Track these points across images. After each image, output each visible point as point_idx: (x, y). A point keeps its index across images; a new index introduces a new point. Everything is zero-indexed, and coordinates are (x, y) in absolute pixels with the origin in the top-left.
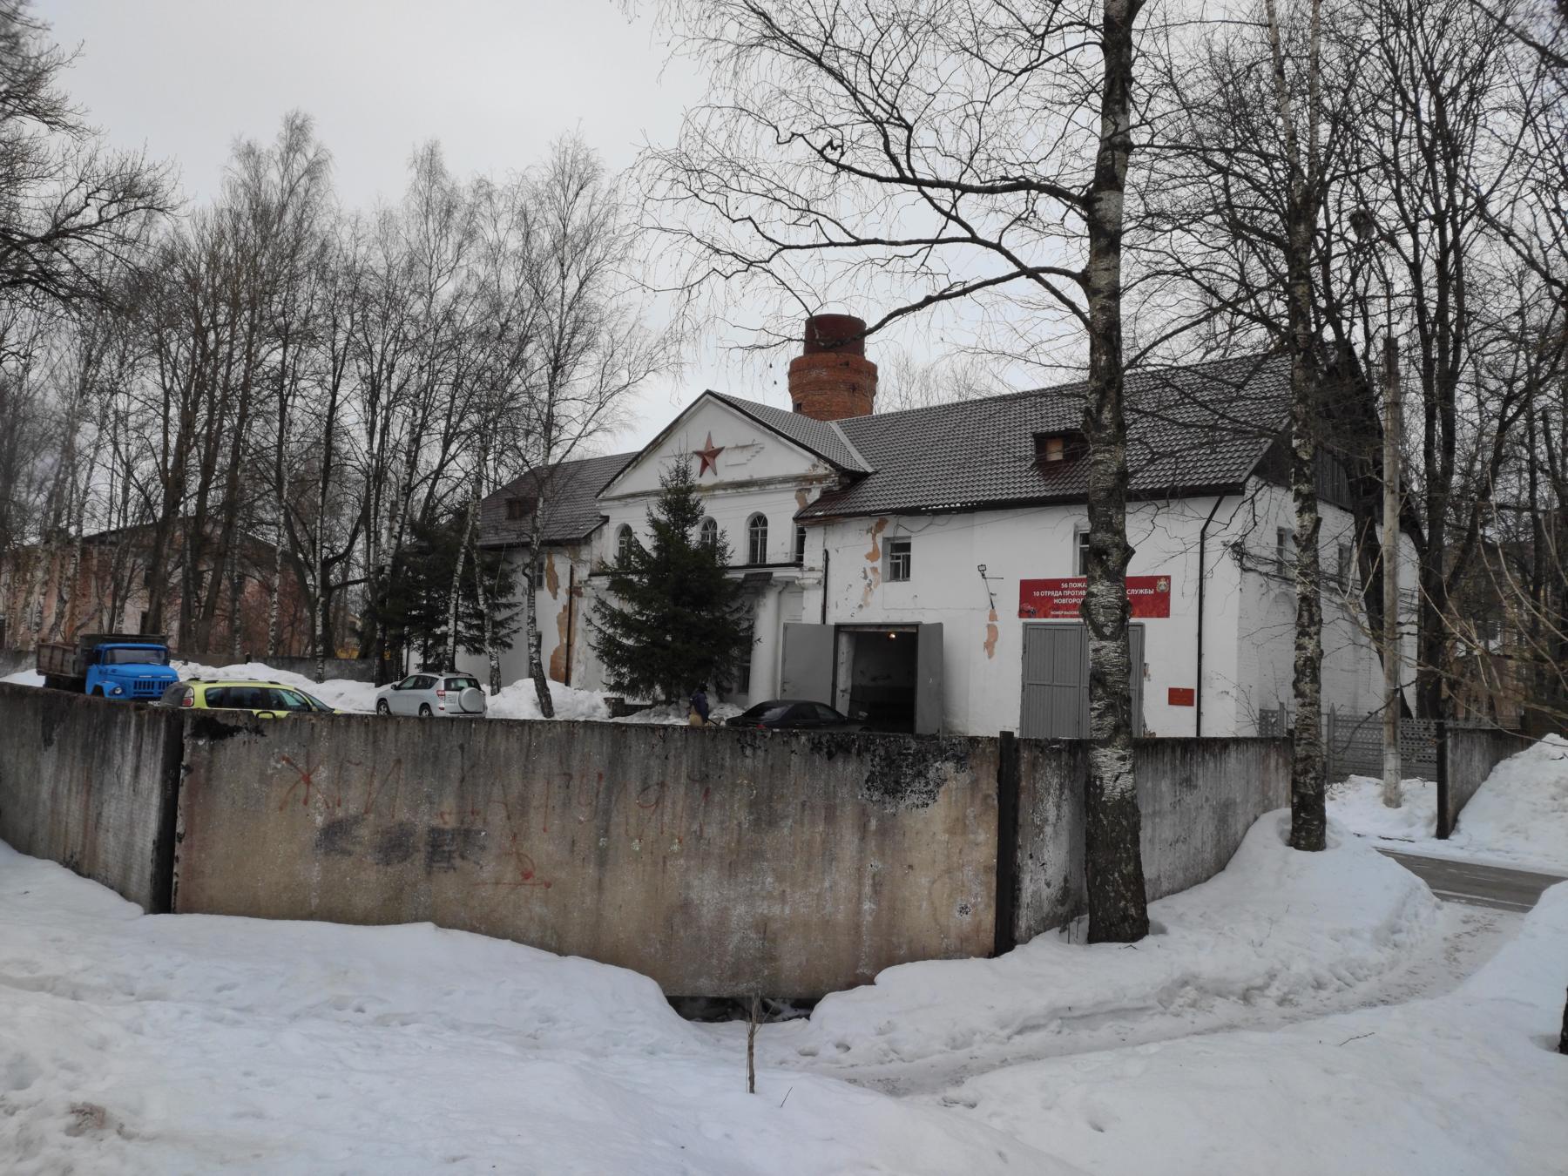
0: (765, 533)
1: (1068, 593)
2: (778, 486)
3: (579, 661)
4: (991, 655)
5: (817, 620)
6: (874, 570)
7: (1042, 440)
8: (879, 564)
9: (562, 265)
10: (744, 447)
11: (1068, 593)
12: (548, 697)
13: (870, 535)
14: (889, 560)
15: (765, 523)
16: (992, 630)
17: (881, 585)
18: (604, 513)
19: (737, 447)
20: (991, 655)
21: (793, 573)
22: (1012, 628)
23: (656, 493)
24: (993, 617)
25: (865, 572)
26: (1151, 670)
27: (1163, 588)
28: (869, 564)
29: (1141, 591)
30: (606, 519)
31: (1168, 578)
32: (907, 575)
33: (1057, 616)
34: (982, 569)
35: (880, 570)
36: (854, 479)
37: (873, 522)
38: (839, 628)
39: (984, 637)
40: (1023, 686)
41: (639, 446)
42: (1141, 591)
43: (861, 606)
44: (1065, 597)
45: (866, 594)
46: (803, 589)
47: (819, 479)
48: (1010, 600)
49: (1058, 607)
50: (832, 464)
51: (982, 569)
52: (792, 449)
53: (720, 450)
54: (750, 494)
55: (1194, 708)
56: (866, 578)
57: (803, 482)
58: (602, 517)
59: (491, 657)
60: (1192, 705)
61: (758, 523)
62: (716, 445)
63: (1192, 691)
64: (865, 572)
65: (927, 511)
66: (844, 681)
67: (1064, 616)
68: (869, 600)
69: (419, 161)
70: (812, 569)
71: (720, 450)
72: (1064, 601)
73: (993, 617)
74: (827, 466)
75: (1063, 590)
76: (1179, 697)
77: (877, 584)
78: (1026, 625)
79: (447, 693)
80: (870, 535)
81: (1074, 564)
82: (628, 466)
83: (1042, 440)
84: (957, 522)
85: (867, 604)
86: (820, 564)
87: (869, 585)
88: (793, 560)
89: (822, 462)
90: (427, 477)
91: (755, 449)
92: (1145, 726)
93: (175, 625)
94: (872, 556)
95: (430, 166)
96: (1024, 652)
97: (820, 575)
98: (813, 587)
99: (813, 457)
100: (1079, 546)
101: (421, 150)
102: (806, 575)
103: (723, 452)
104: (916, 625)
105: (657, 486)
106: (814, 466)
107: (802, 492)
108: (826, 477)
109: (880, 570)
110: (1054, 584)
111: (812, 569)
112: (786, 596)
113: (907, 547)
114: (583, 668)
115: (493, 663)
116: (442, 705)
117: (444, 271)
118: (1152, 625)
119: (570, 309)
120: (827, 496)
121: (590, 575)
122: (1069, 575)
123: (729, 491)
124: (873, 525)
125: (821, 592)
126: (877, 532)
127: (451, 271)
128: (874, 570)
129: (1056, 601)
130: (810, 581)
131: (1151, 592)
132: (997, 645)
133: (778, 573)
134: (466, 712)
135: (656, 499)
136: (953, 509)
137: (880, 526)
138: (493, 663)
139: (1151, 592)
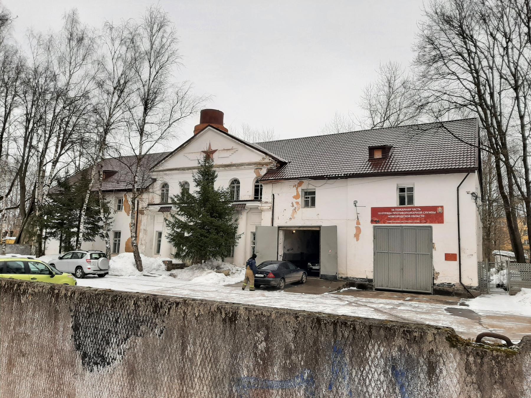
0: (238, 187)
1: (395, 213)
2: (246, 167)
3: (142, 244)
4: (358, 240)
5: (270, 224)
6: (297, 203)
7: (372, 150)
8: (299, 200)
9: (150, 62)
10: (228, 150)
11: (395, 213)
12: (140, 261)
13: (295, 188)
14: (303, 198)
15: (239, 183)
16: (358, 230)
17: (301, 209)
18: (153, 177)
19: (224, 150)
20: (358, 240)
21: (257, 204)
22: (368, 229)
23: (197, 168)
24: (358, 223)
25: (292, 203)
26: (436, 246)
27: (440, 211)
28: (294, 201)
29: (430, 212)
30: (155, 180)
31: (442, 207)
32: (313, 204)
33: (390, 223)
34: (355, 203)
35: (300, 203)
36: (282, 164)
37: (297, 182)
38: (279, 228)
39: (354, 231)
40: (374, 253)
41: (172, 150)
42: (430, 212)
43: (291, 218)
44: (394, 215)
45: (293, 213)
46: (261, 211)
47: (267, 164)
48: (367, 216)
49: (390, 219)
50: (273, 158)
51: (355, 203)
52: (253, 151)
53: (215, 151)
54: (231, 170)
55: (457, 262)
56: (293, 206)
57: (259, 165)
58: (152, 179)
59: (106, 242)
60: (456, 260)
61: (235, 182)
62: (213, 148)
63: (456, 255)
64: (292, 203)
65: (327, 177)
66: (281, 252)
67: (393, 223)
68: (295, 216)
69: (67, 16)
70: (266, 203)
71: (215, 151)
72: (393, 216)
73: (358, 223)
74: (271, 158)
75: (392, 212)
76: (449, 257)
77: (299, 209)
78: (374, 227)
79: (92, 261)
80: (295, 188)
81: (397, 201)
82: (167, 157)
83: (372, 150)
84: (339, 181)
85: (294, 218)
86: (270, 200)
87: (295, 209)
88: (253, 199)
89: (268, 157)
90: (513, 32)
91: (232, 152)
92: (434, 270)
93: (500, 142)
94: (296, 197)
95: (73, 20)
96: (374, 238)
97: (271, 205)
98: (268, 210)
99: (264, 154)
100: (398, 193)
101: (69, 11)
102: (263, 205)
103: (217, 151)
104: (320, 227)
105: (196, 164)
106: (263, 158)
107: (257, 169)
108: (271, 163)
109: (300, 203)
110: (389, 209)
111: (266, 203)
112: (249, 213)
113: (314, 193)
114: (144, 247)
115: (107, 246)
116: (89, 267)
117: (78, 65)
118: (436, 227)
119: (153, 82)
120: (270, 172)
121: (149, 205)
122: (396, 206)
123: (221, 169)
124: (297, 184)
125: (271, 213)
126: (298, 186)
127: (81, 65)
128: (297, 203)
129: (389, 216)
130: (266, 208)
131: (435, 213)
132: (360, 235)
133: (248, 204)
134: (101, 270)
135: (196, 171)
136: (339, 177)
137: (300, 184)
138: (107, 246)
139: (435, 213)
